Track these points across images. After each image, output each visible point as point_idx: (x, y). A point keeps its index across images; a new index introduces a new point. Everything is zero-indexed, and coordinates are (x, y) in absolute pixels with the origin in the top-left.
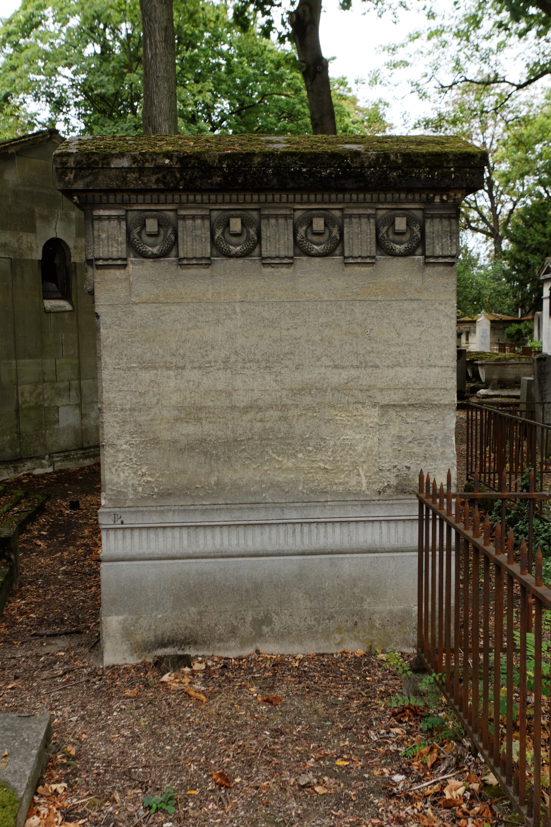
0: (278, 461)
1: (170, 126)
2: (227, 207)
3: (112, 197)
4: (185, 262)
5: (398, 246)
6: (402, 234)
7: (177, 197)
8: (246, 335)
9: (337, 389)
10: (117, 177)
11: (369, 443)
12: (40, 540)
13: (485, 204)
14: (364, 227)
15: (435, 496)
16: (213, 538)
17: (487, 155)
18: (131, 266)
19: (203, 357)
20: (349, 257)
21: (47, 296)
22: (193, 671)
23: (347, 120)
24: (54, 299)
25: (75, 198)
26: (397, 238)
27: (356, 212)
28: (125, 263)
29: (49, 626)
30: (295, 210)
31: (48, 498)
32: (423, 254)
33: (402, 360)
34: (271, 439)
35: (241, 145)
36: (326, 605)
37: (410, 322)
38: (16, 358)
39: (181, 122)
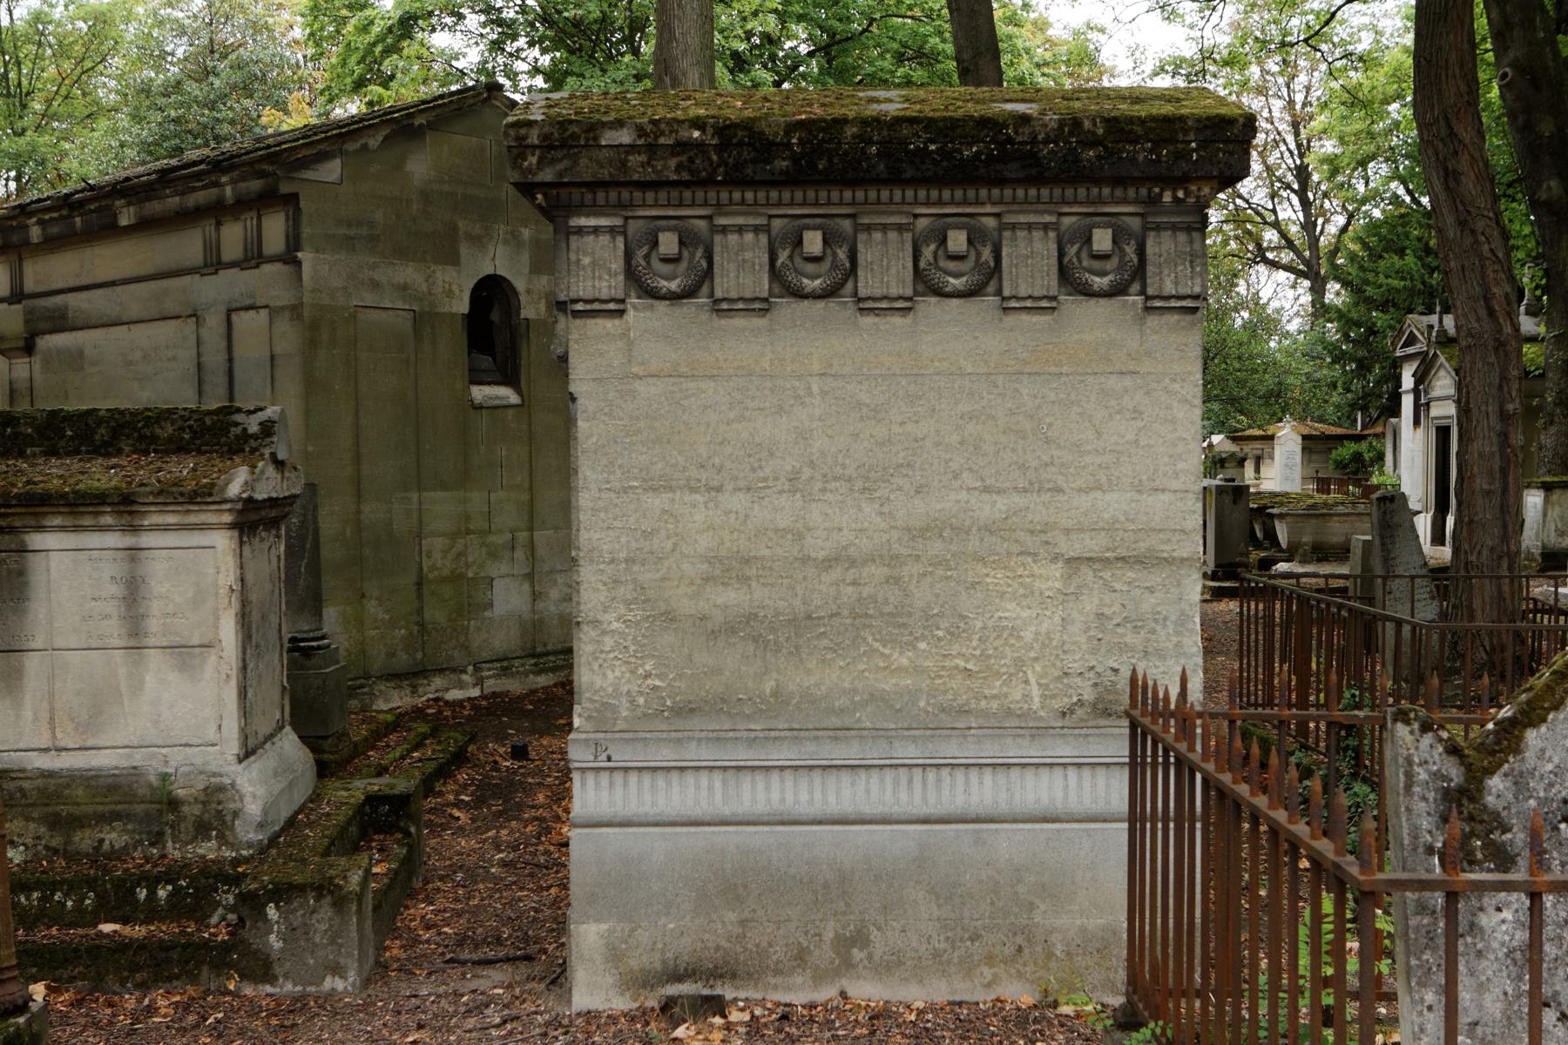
0: (882, 654)
1: (702, 75)
2: (798, 212)
3: (601, 196)
4: (725, 306)
5: (1097, 279)
6: (1105, 257)
7: (712, 194)
8: (830, 432)
9: (989, 529)
10: (610, 161)
11: (1045, 625)
12: (459, 809)
13: (1294, 217)
14: (1038, 245)
15: (1155, 714)
16: (768, 789)
17: (1255, 120)
18: (631, 313)
19: (753, 470)
20: (1010, 298)
21: (477, 377)
22: (729, 1023)
23: (1025, 66)
24: (489, 383)
25: (539, 196)
26: (1096, 265)
27: (1022, 219)
28: (621, 307)
29: (476, 946)
30: (916, 216)
31: (473, 739)
32: (1143, 292)
33: (1104, 480)
34: (871, 616)
35: (823, 105)
36: (967, 914)
37: (1119, 412)
38: (420, 488)
39: (720, 70)
